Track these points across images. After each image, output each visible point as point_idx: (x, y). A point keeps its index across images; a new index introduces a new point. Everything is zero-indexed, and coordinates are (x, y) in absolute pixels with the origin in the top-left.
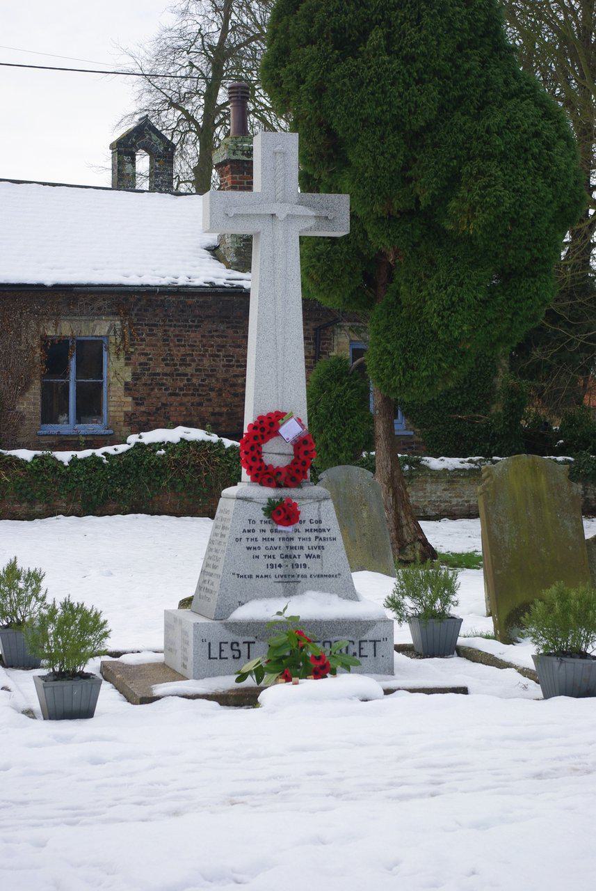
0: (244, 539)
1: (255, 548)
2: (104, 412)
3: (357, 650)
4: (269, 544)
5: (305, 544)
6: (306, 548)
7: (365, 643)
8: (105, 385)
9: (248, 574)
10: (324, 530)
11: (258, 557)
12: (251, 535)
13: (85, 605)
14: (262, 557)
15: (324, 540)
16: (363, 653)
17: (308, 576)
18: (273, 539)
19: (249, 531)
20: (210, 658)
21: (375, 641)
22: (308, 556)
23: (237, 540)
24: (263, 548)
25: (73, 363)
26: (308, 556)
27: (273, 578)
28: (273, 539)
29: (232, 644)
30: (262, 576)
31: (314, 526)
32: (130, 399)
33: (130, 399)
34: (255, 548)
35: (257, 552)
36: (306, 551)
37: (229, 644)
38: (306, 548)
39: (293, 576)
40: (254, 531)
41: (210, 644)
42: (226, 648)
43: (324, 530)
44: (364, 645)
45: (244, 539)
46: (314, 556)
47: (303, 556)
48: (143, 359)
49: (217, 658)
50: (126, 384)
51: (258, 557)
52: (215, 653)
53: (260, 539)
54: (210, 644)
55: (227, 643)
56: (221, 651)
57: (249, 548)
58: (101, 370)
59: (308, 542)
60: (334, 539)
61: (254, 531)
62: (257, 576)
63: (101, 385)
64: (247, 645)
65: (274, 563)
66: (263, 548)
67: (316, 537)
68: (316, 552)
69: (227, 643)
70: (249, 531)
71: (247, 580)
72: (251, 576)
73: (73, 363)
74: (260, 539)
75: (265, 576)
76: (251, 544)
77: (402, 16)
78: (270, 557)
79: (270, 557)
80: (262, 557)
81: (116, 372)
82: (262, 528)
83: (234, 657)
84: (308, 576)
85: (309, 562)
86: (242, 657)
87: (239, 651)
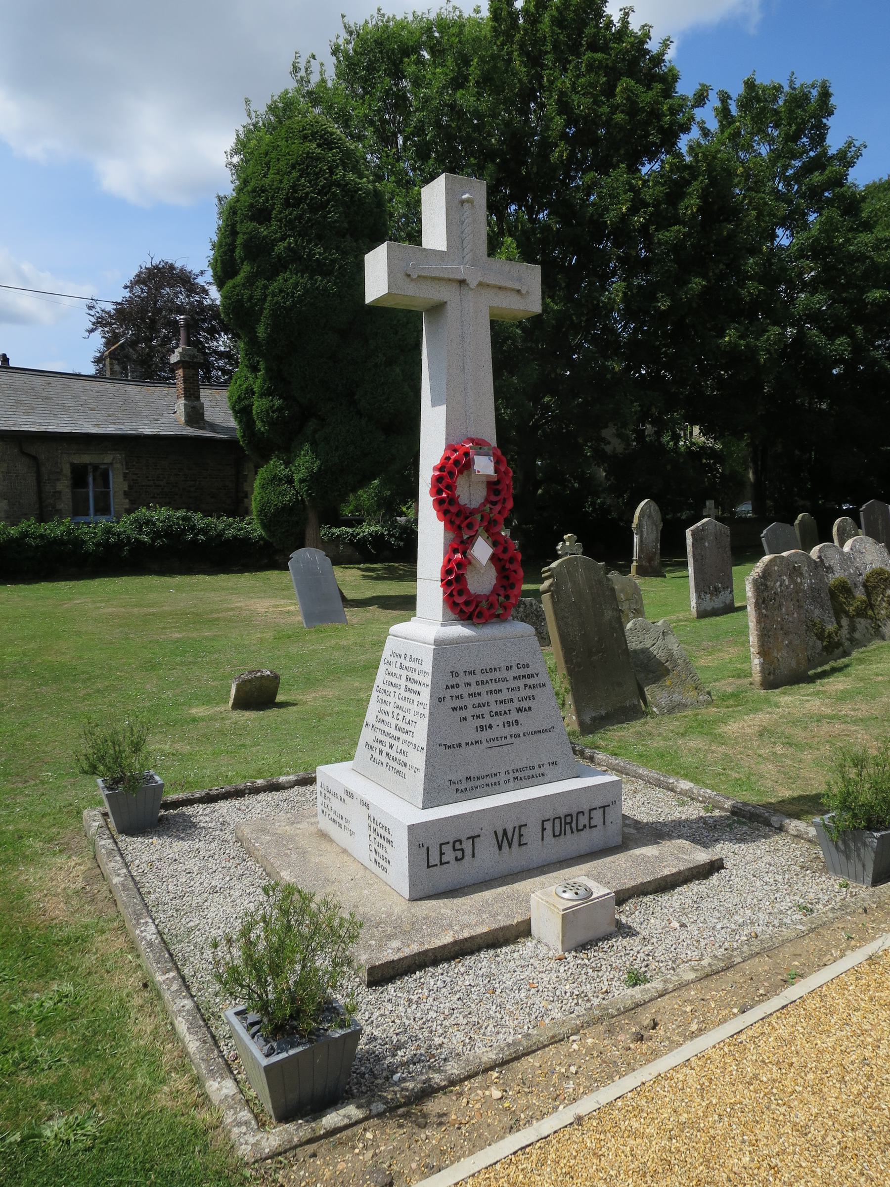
0: (448, 699)
1: (461, 708)
2: (112, 509)
3: (586, 822)
4: (476, 700)
5: (514, 695)
6: (516, 700)
7: (595, 811)
8: (111, 493)
9: (455, 743)
10: (532, 676)
11: (465, 719)
12: (455, 692)
13: (361, 910)
14: (470, 718)
15: (495, 669)
16: (593, 823)
17: (522, 735)
18: (479, 694)
19: (452, 687)
20: (429, 867)
21: (604, 807)
22: (519, 710)
23: (440, 700)
24: (470, 707)
25: (91, 479)
26: (519, 710)
27: (485, 744)
28: (479, 694)
29: (454, 842)
30: (472, 743)
31: (522, 672)
32: (127, 501)
33: (127, 501)
34: (461, 708)
35: (463, 713)
36: (517, 704)
37: (451, 844)
38: (516, 700)
39: (506, 738)
40: (458, 686)
41: (428, 848)
42: (447, 849)
43: (532, 676)
44: (594, 813)
45: (448, 699)
46: (525, 710)
47: (514, 711)
48: (134, 477)
49: (436, 865)
50: (125, 492)
51: (465, 719)
52: (435, 859)
53: (465, 695)
54: (428, 848)
55: (448, 843)
56: (442, 854)
57: (454, 709)
58: (108, 483)
59: (517, 693)
60: (544, 685)
61: (458, 686)
62: (467, 744)
63: (108, 493)
64: (471, 841)
65: (483, 724)
66: (470, 707)
67: (526, 686)
68: (525, 704)
69: (448, 843)
70: (452, 687)
71: (457, 751)
72: (460, 745)
73: (91, 479)
74: (465, 695)
75: (476, 742)
76: (457, 703)
77: (503, 120)
78: (478, 717)
79: (478, 717)
80: (470, 718)
81: (117, 484)
82: (467, 681)
83: (457, 859)
84: (522, 735)
85: (520, 717)
86: (466, 857)
87: (462, 850)
